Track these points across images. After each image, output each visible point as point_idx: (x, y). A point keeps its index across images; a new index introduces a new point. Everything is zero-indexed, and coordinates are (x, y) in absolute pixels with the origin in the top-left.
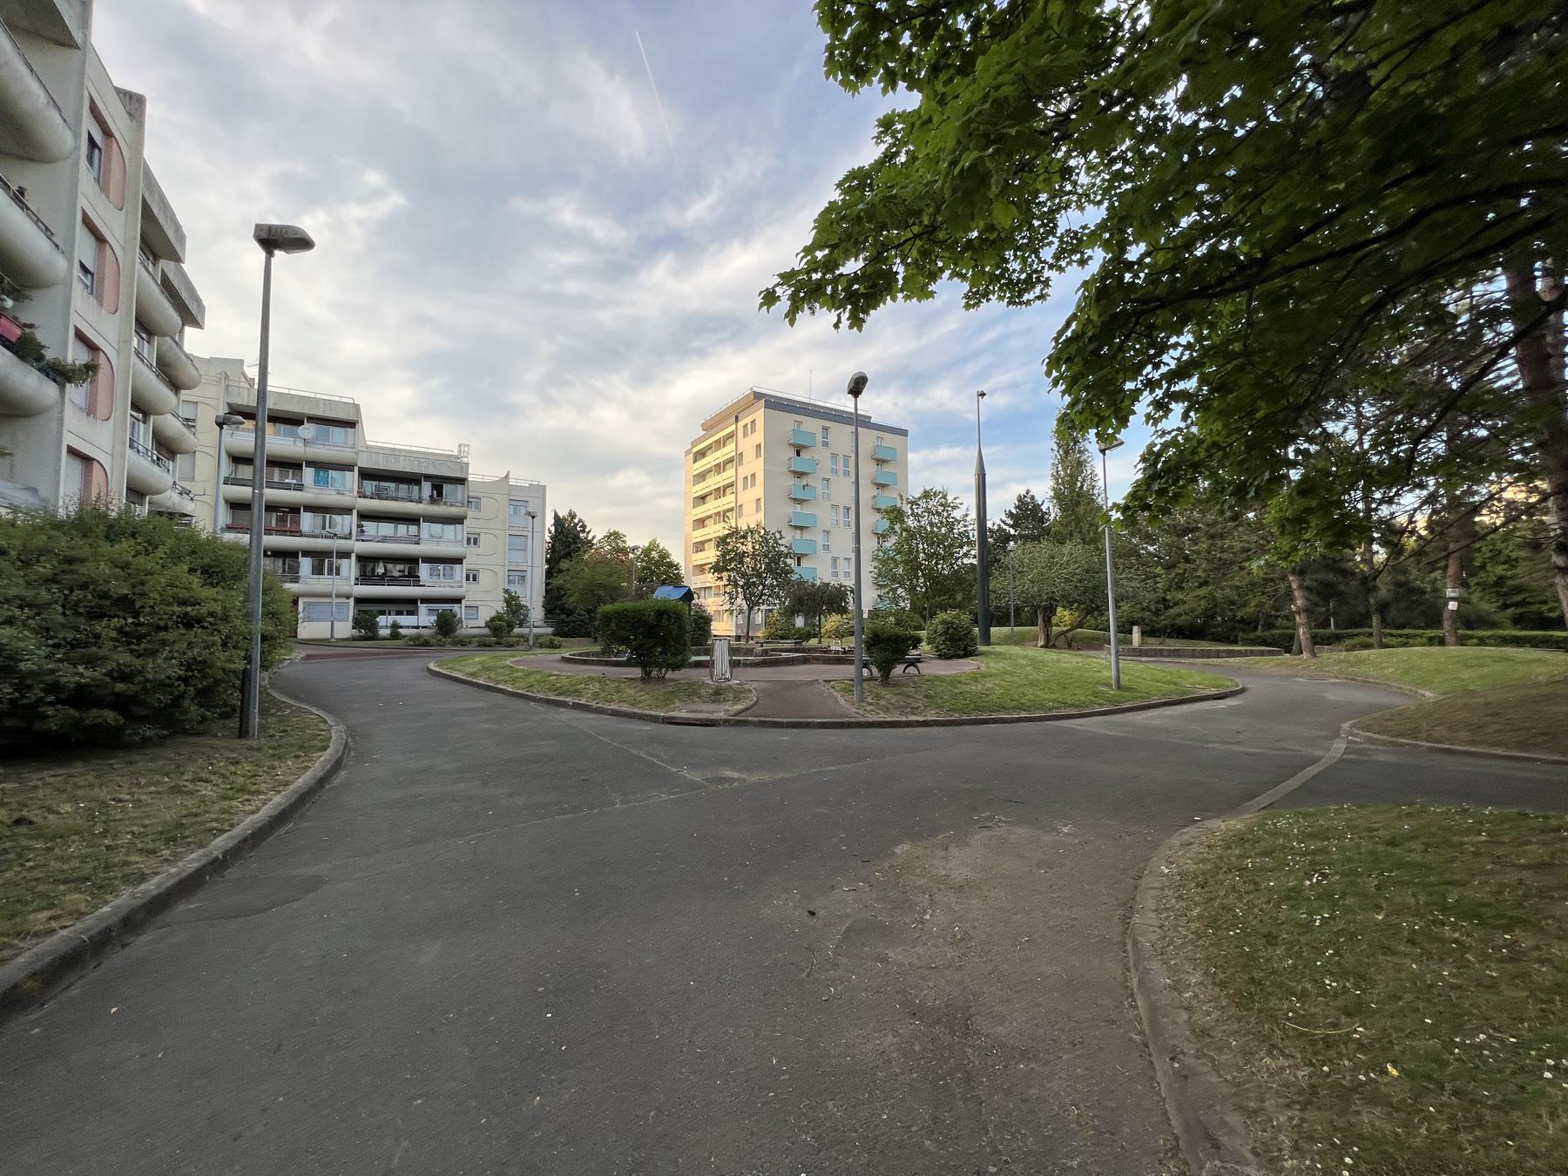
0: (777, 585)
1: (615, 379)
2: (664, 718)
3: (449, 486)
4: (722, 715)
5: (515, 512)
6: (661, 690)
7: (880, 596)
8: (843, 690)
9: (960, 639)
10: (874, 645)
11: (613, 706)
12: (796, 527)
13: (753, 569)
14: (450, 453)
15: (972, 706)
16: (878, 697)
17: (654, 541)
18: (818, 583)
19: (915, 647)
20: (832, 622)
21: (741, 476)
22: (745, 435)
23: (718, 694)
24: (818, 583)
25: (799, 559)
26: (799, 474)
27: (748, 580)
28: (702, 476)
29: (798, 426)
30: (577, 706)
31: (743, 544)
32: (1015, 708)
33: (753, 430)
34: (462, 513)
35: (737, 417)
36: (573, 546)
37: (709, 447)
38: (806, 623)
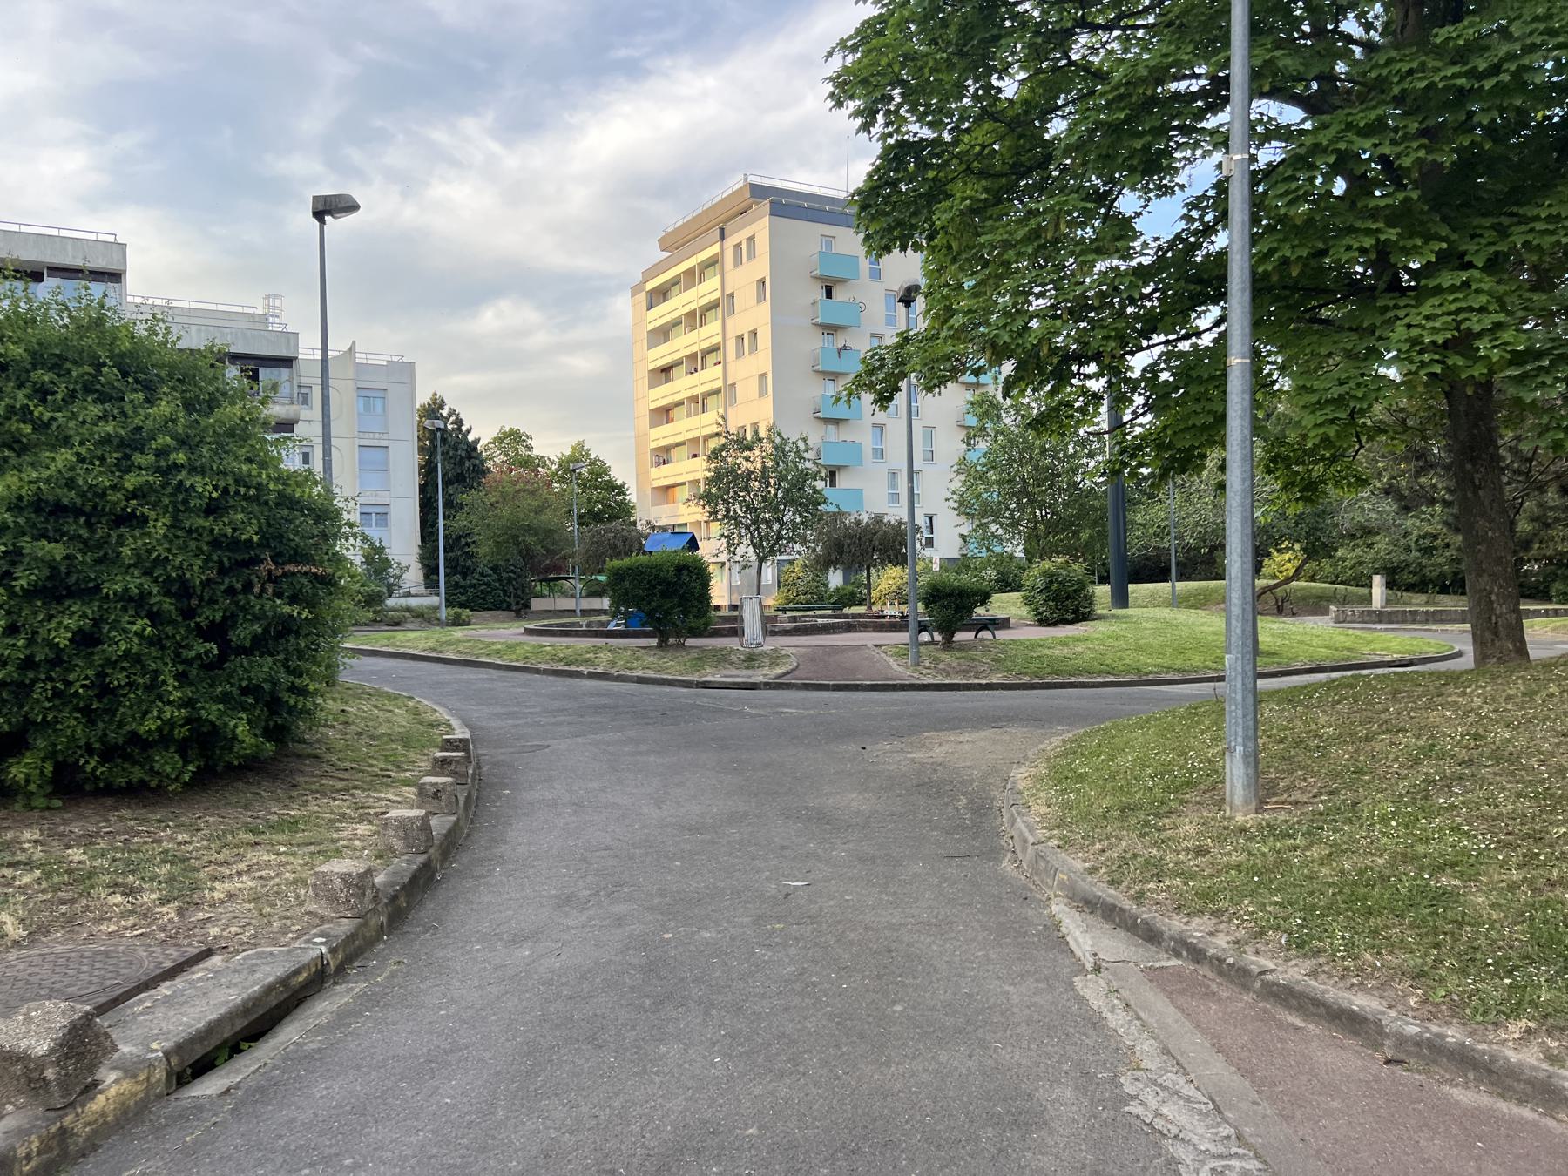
0: (802, 523)
1: (470, 125)
2: (698, 683)
3: (268, 370)
4: (761, 679)
5: (367, 408)
6: (684, 656)
7: (963, 537)
8: (898, 654)
9: (1068, 598)
10: (933, 602)
11: (639, 673)
12: (827, 421)
13: (765, 499)
14: (251, 311)
15: (1049, 670)
16: (937, 661)
17: (581, 445)
18: (865, 518)
19: (983, 603)
20: (888, 578)
21: (732, 333)
22: (738, 262)
23: (751, 660)
24: (865, 518)
25: (832, 475)
26: (830, 329)
27: (758, 516)
28: (663, 334)
29: (829, 244)
30: (593, 676)
31: (747, 459)
32: (1100, 672)
33: (752, 254)
34: (292, 416)
35: (722, 230)
36: (467, 464)
37: (675, 282)
38: (846, 580)
